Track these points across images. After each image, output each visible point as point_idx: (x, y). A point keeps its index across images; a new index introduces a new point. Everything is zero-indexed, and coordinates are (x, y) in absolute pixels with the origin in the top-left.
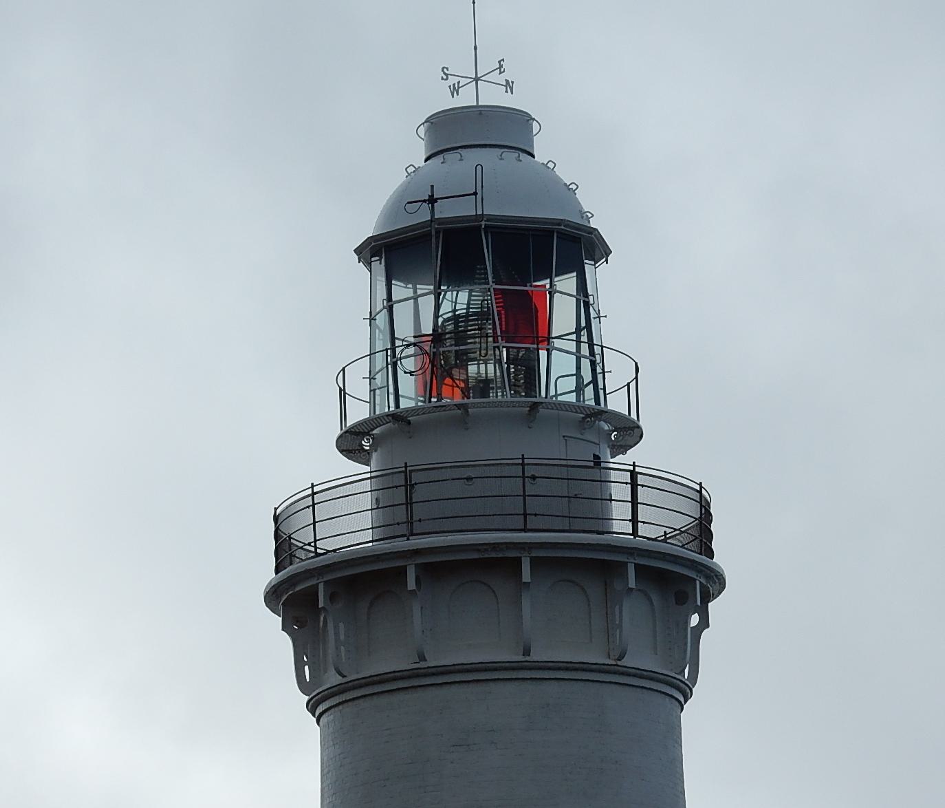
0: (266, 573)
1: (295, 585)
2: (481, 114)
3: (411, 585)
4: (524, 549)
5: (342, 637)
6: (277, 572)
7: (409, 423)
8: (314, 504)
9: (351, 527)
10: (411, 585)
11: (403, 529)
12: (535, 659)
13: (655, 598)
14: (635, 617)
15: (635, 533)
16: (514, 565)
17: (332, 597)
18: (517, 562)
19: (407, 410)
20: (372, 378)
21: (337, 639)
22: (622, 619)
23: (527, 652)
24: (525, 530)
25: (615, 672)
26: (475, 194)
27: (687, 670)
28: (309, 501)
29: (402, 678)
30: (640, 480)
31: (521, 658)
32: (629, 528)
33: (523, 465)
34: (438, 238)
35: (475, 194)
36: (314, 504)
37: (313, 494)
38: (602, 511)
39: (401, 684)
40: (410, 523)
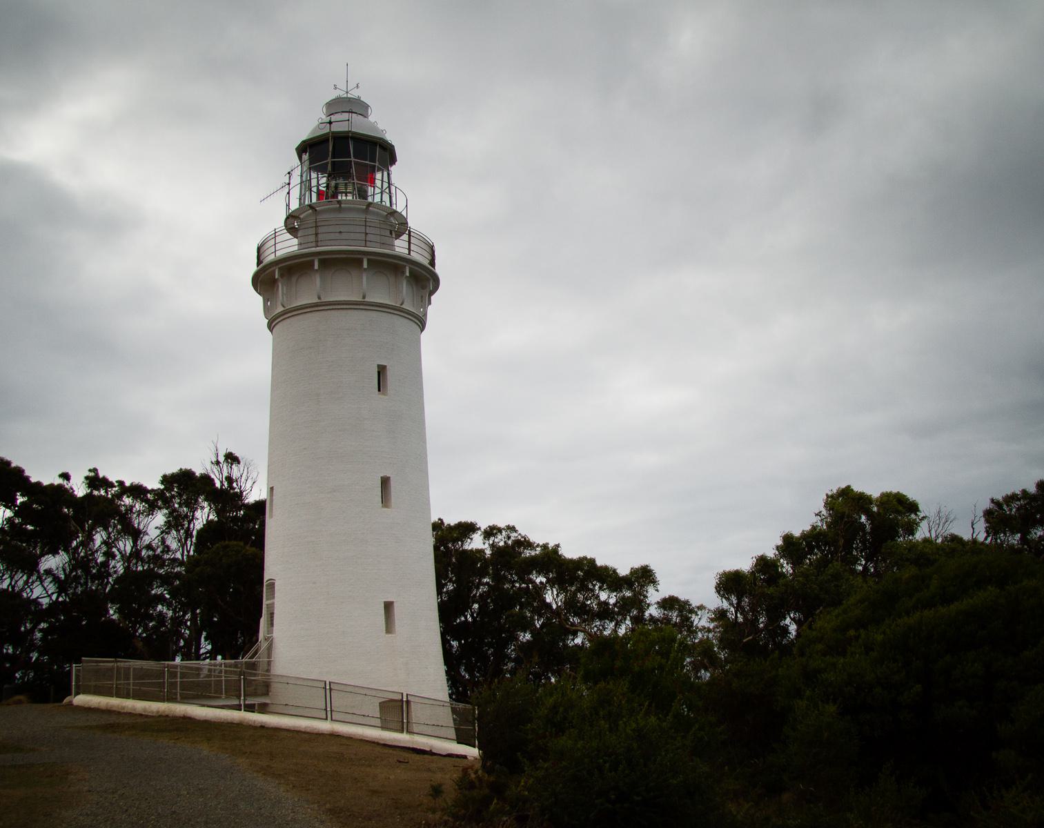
0: (253, 268)
1: (265, 271)
2: (349, 100)
3: (316, 267)
4: (364, 255)
5: (285, 292)
6: (258, 266)
7: (316, 210)
8: (275, 237)
9: (289, 245)
10: (316, 267)
11: (314, 244)
12: (368, 300)
13: (415, 289)
14: (405, 294)
15: (409, 254)
16: (360, 262)
17: (282, 275)
18: (361, 261)
19: (314, 203)
20: (302, 176)
21: (283, 293)
22: (418, 753)
23: (364, 297)
24: (366, 246)
25: (399, 311)
26: (348, 120)
27: (477, 742)
28: (273, 236)
29: (310, 307)
30: (412, 234)
31: (360, 300)
32: (407, 252)
33: (365, 221)
34: (119, 661)
35: (348, 120)
36: (275, 237)
37: (276, 232)
38: (408, 722)
39: (309, 310)
40: (317, 241)
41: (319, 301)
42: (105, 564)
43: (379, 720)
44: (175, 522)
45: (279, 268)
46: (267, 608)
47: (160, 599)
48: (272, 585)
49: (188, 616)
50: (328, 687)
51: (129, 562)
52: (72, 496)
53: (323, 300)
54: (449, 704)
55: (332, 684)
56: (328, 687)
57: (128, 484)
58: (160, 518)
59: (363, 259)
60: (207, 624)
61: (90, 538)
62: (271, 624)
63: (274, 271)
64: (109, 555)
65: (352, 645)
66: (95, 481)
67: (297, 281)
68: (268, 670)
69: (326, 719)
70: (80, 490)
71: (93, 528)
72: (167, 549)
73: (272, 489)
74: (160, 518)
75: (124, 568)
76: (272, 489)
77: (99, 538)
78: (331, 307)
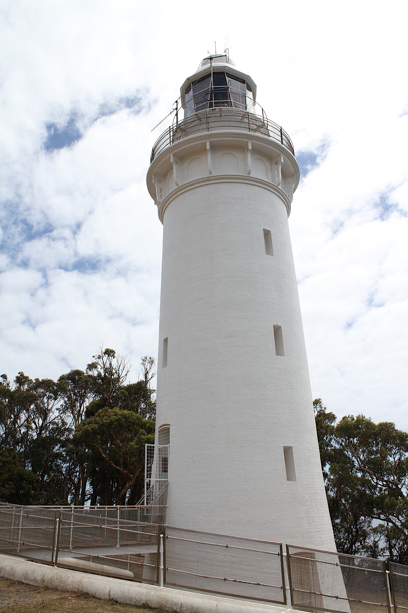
26: (226, 56)
28: (169, 129)
35: (226, 56)
41: (210, 176)
42: (26, 434)
43: (347, 601)
44: (70, 406)
45: (174, 155)
46: (159, 450)
47: (58, 456)
48: (166, 431)
49: (78, 469)
50: (285, 554)
51: (41, 431)
52: (9, 391)
53: (213, 175)
54: (337, 561)
55: (290, 548)
56: (285, 554)
57: (40, 380)
58: (60, 402)
59: (248, 142)
60: (92, 474)
61: (17, 417)
62: (165, 469)
63: (170, 157)
64: (28, 427)
65: (247, 493)
66: (21, 379)
67: (189, 164)
68: (161, 518)
69: (285, 603)
70: (13, 387)
71: (19, 412)
72: (64, 423)
73: (166, 340)
74: (60, 402)
75: (37, 434)
76: (166, 340)
77: (23, 417)
78: (221, 181)
